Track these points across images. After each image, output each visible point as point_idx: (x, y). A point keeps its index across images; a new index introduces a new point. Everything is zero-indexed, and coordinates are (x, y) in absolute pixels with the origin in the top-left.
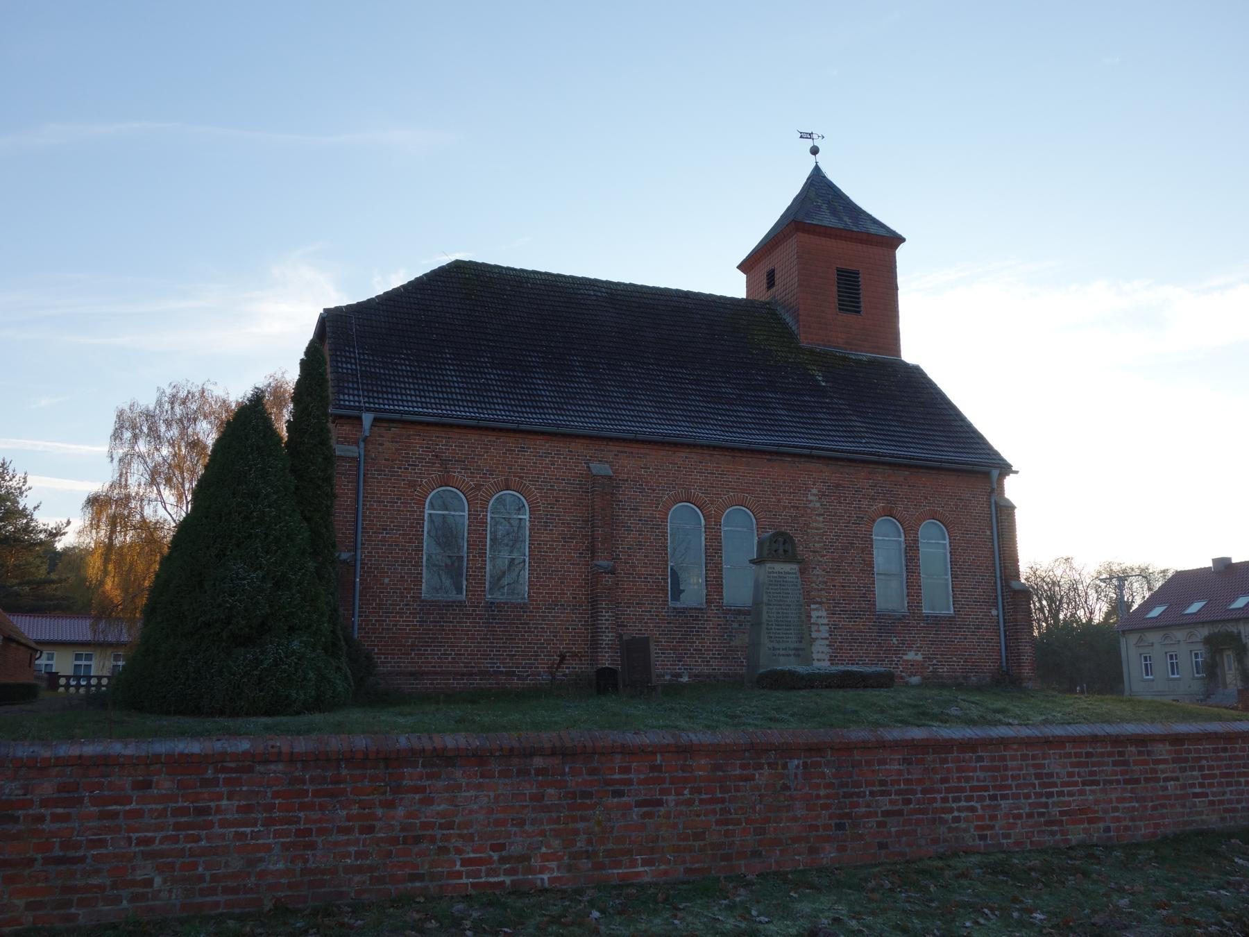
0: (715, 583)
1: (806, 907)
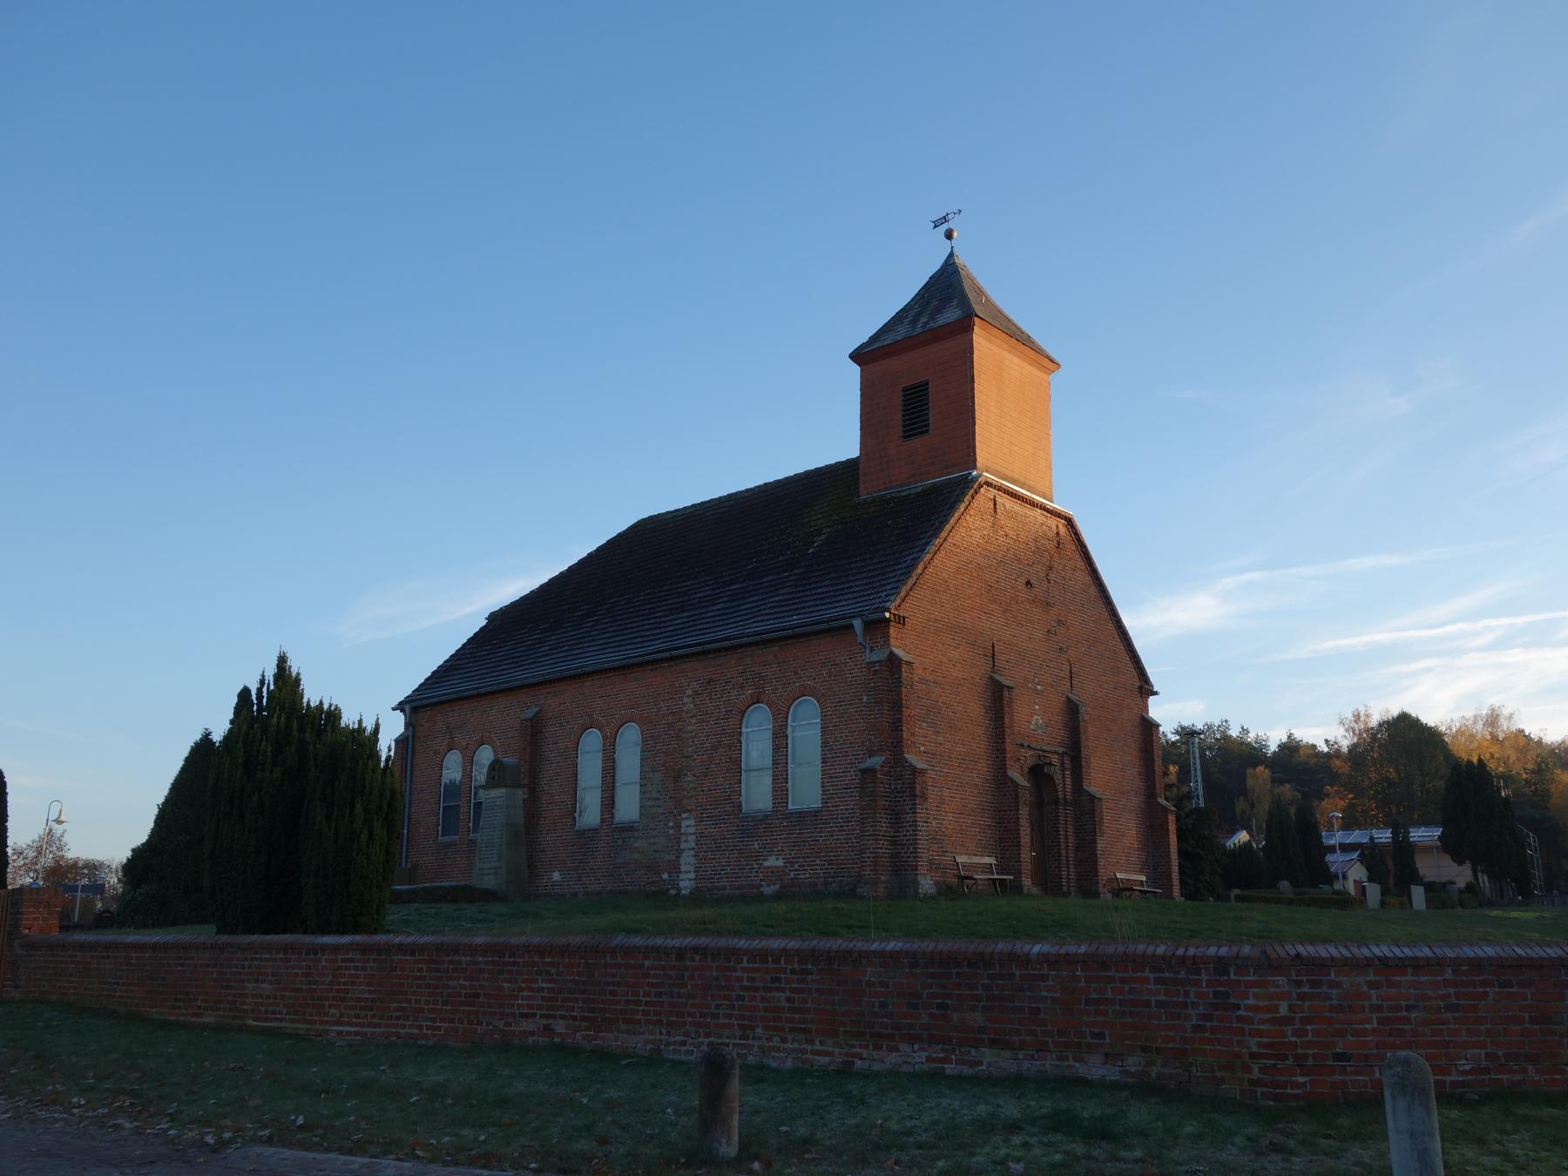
0: (609, 803)
1: (1058, 1157)
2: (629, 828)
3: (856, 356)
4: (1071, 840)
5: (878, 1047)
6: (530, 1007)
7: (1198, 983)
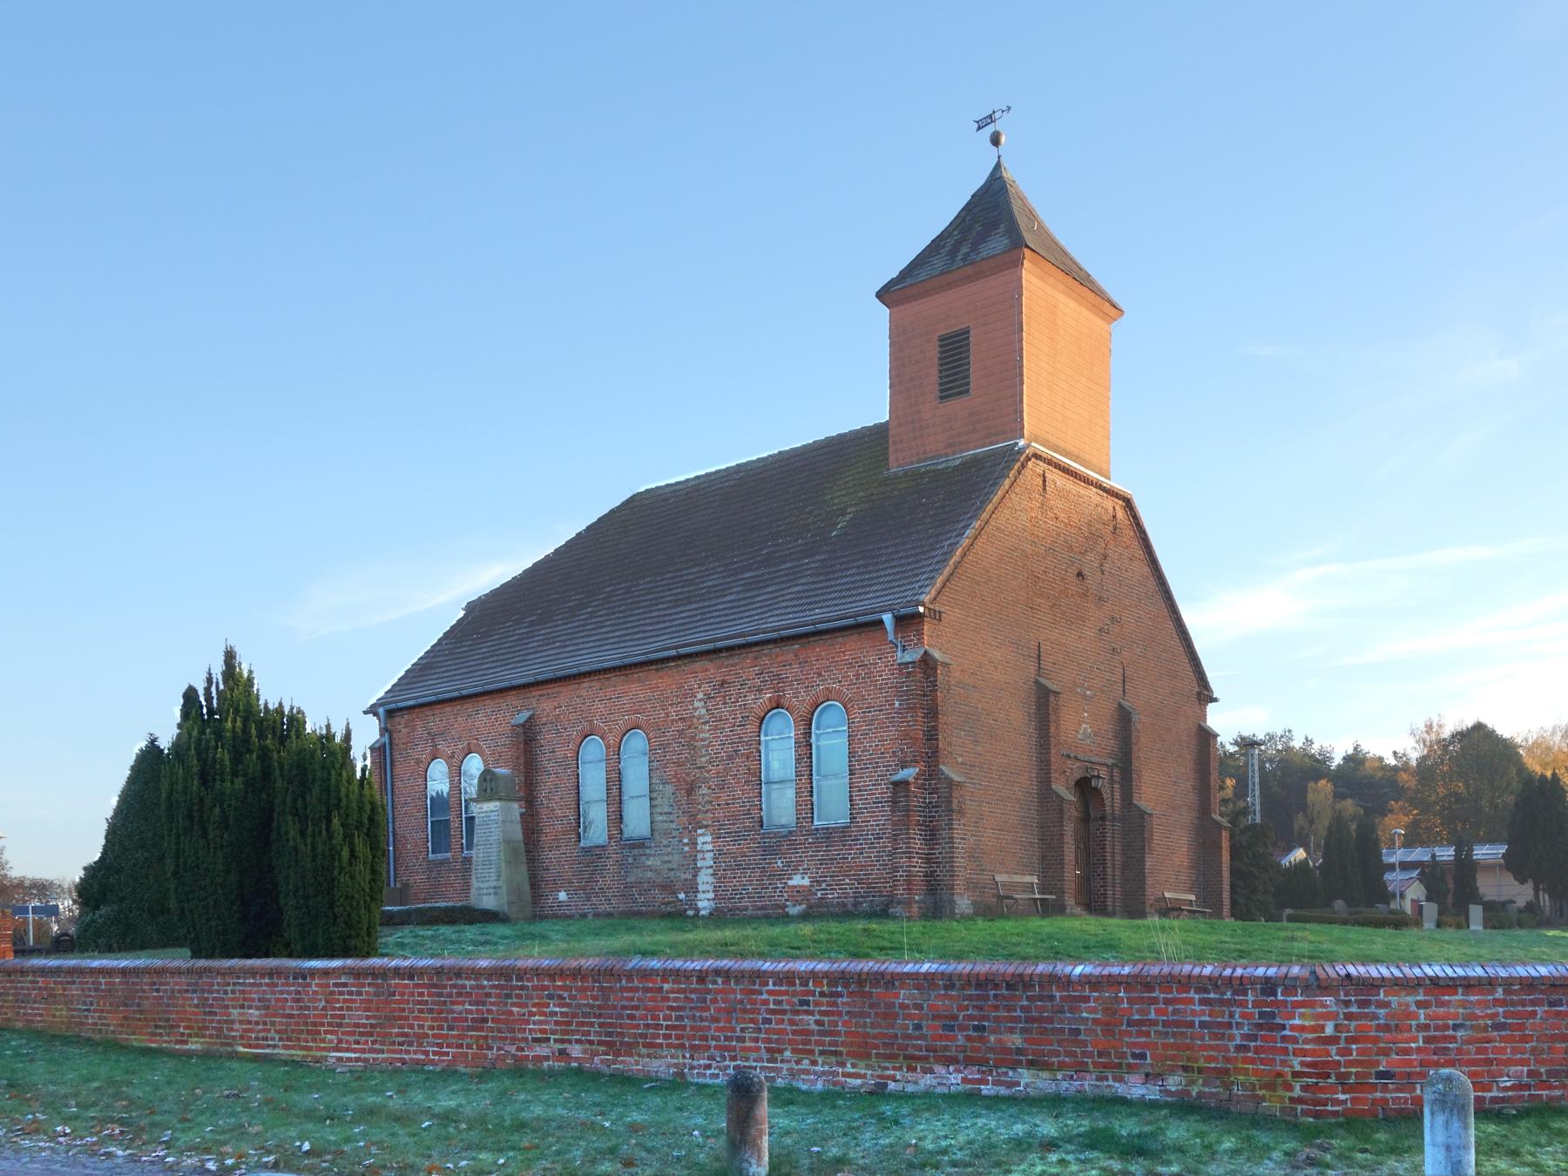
0: (617, 818)
2: (639, 844)
4: (1118, 857)
5: (911, 1069)
7: (1243, 1004)
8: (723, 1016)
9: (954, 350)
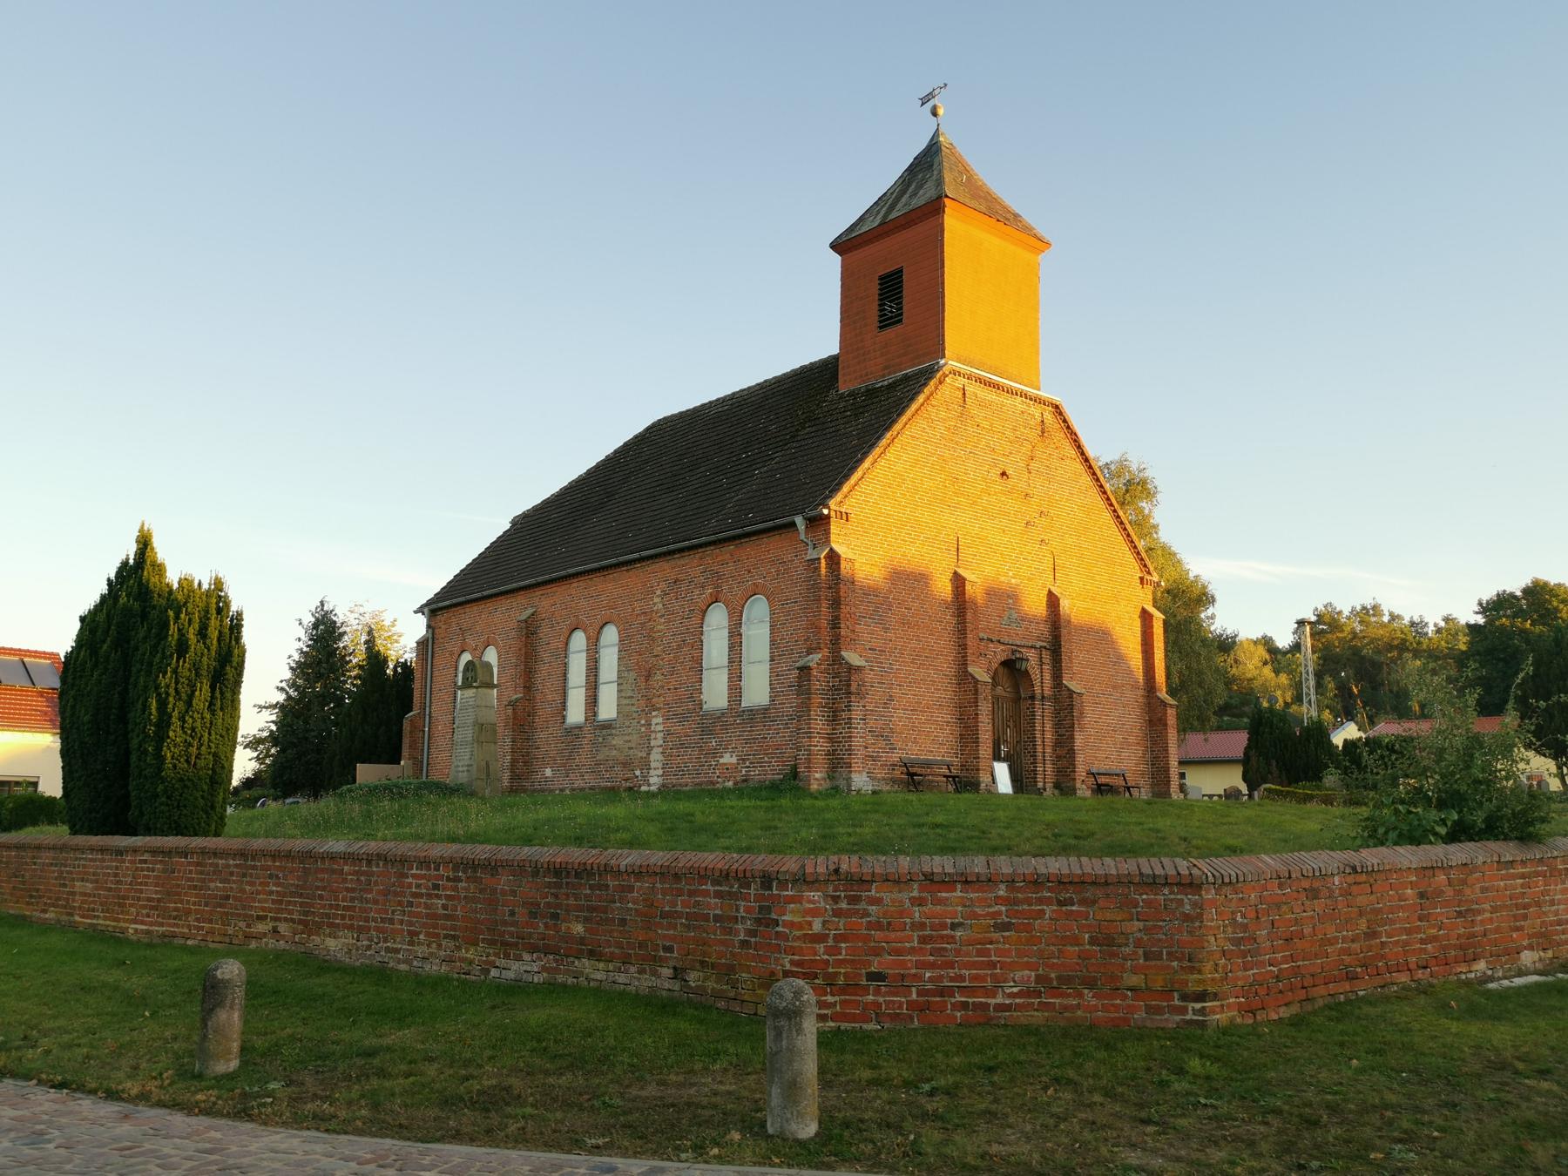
0: (735, 689)
2: (607, 726)
3: (835, 246)
4: (1048, 735)
5: (507, 956)
6: (263, 909)
7: (746, 898)
8: (381, 898)
9: (891, 286)
